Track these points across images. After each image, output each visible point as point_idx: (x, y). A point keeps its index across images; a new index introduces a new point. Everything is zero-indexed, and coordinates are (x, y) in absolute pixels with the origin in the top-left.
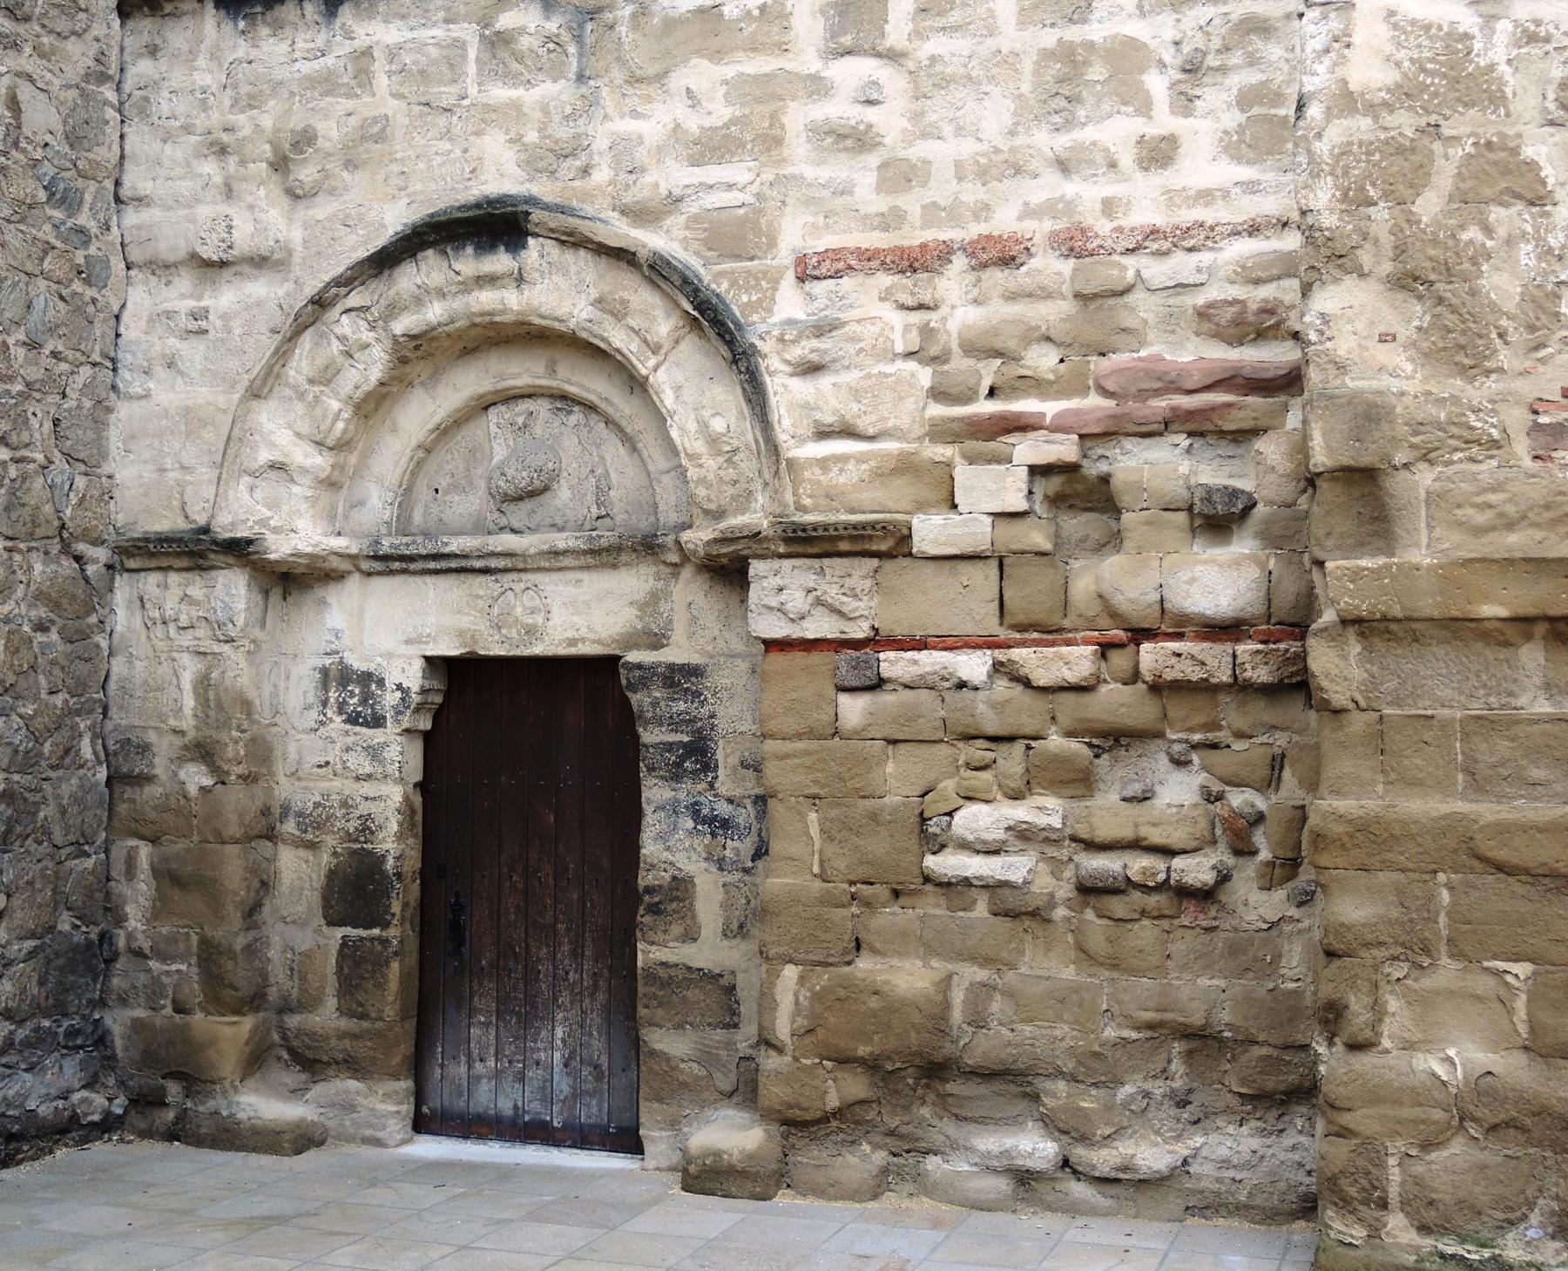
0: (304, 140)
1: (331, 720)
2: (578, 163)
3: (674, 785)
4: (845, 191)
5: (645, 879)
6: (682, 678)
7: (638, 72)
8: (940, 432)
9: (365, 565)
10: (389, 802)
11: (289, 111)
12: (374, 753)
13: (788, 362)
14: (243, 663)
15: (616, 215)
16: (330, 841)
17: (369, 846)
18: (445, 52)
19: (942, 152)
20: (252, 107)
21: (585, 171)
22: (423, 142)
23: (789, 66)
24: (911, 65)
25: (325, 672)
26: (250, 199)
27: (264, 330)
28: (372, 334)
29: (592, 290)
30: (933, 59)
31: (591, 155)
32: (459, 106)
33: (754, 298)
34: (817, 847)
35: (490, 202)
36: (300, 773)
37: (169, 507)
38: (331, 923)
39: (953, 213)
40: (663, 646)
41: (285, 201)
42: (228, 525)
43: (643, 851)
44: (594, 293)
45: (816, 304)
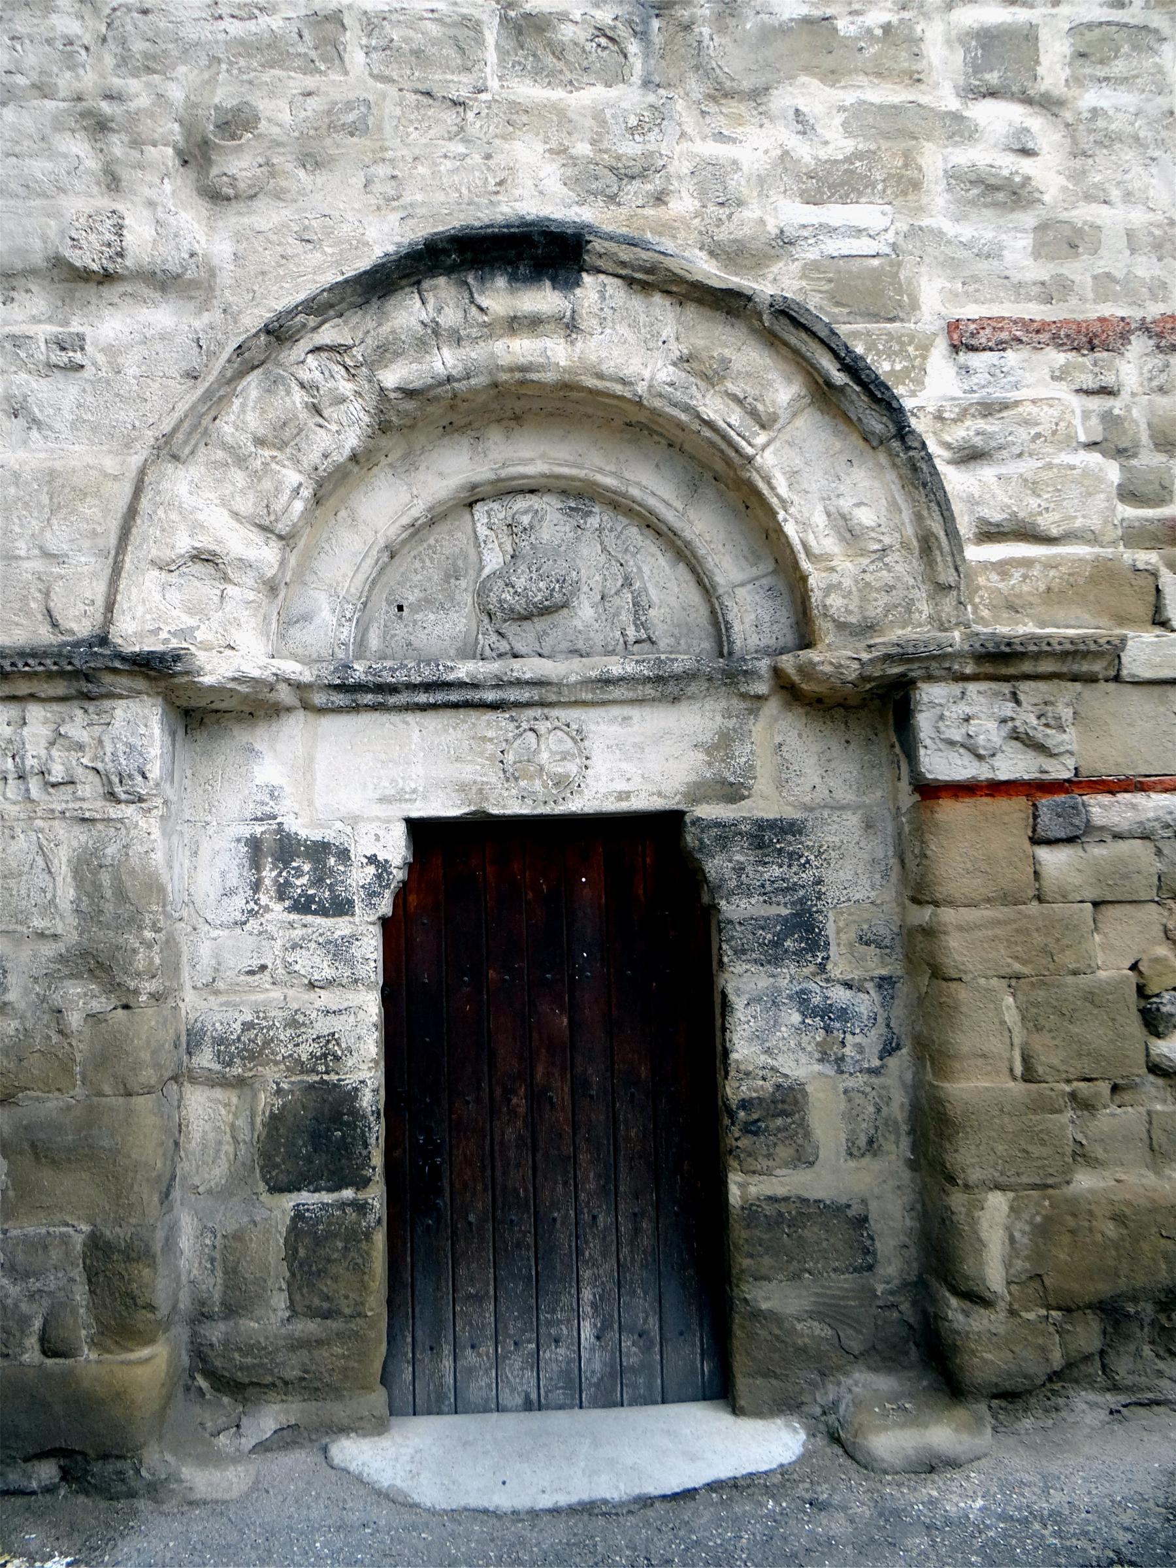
0: (236, 123)
1: (267, 909)
2: (649, 187)
3: (770, 969)
4: (992, 253)
5: (735, 1090)
6: (770, 837)
7: (728, 83)
8: (1135, 536)
9: (319, 699)
10: (361, 1014)
11: (212, 81)
12: (338, 950)
13: (948, 446)
14: (156, 833)
15: (703, 255)
16: (271, 1074)
17: (334, 1077)
18: (452, 32)
19: (1112, 217)
20: (149, 70)
21: (659, 199)
22: (423, 141)
23: (924, 100)
24: (1068, 116)
25: (255, 845)
26: (147, 192)
27: (173, 371)
28: (350, 386)
29: (673, 345)
30: (1095, 112)
31: (668, 178)
32: (476, 99)
33: (898, 367)
34: (1017, 1041)
35: (525, 224)
36: (220, 985)
37: (29, 614)
38: (277, 1189)
39: (1129, 289)
40: (743, 798)
41: (203, 206)
42: (134, 632)
43: (734, 1056)
44: (676, 349)
45: (974, 380)
